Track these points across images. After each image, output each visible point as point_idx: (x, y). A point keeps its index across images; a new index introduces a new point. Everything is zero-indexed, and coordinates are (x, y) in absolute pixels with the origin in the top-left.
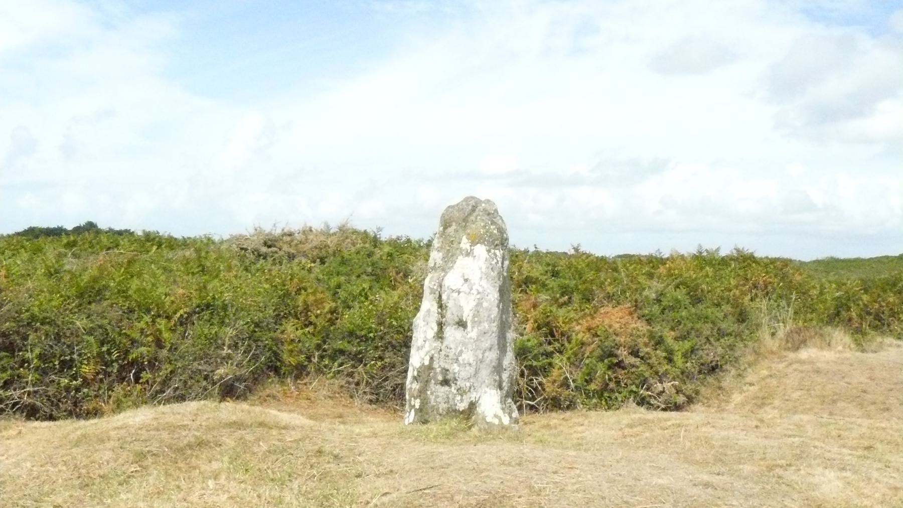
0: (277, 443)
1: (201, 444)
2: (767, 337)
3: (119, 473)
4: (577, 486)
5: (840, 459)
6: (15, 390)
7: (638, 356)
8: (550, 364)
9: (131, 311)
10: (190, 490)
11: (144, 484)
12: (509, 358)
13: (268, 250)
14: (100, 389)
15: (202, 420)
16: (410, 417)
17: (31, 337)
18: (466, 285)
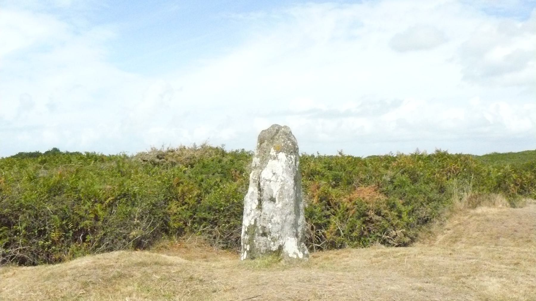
0: (166, 274)
1: (121, 276)
3: (73, 295)
4: (343, 293)
5: (499, 271)
6: (12, 249)
7: (380, 215)
8: (329, 222)
9: (80, 199)
12: (302, 219)
13: (159, 160)
14: (62, 246)
15: (122, 261)
16: (244, 256)
17: (20, 217)
18: (274, 177)
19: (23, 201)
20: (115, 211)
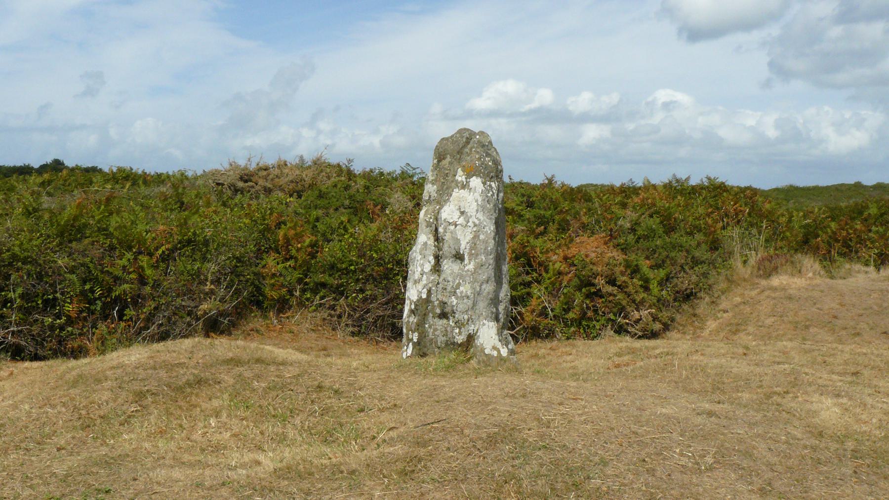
0: (276, 379)
2: (739, 264)
3: (120, 413)
8: (529, 294)
9: (112, 248)
14: (84, 326)
17: (13, 277)
19: (17, 249)
20: (173, 269)
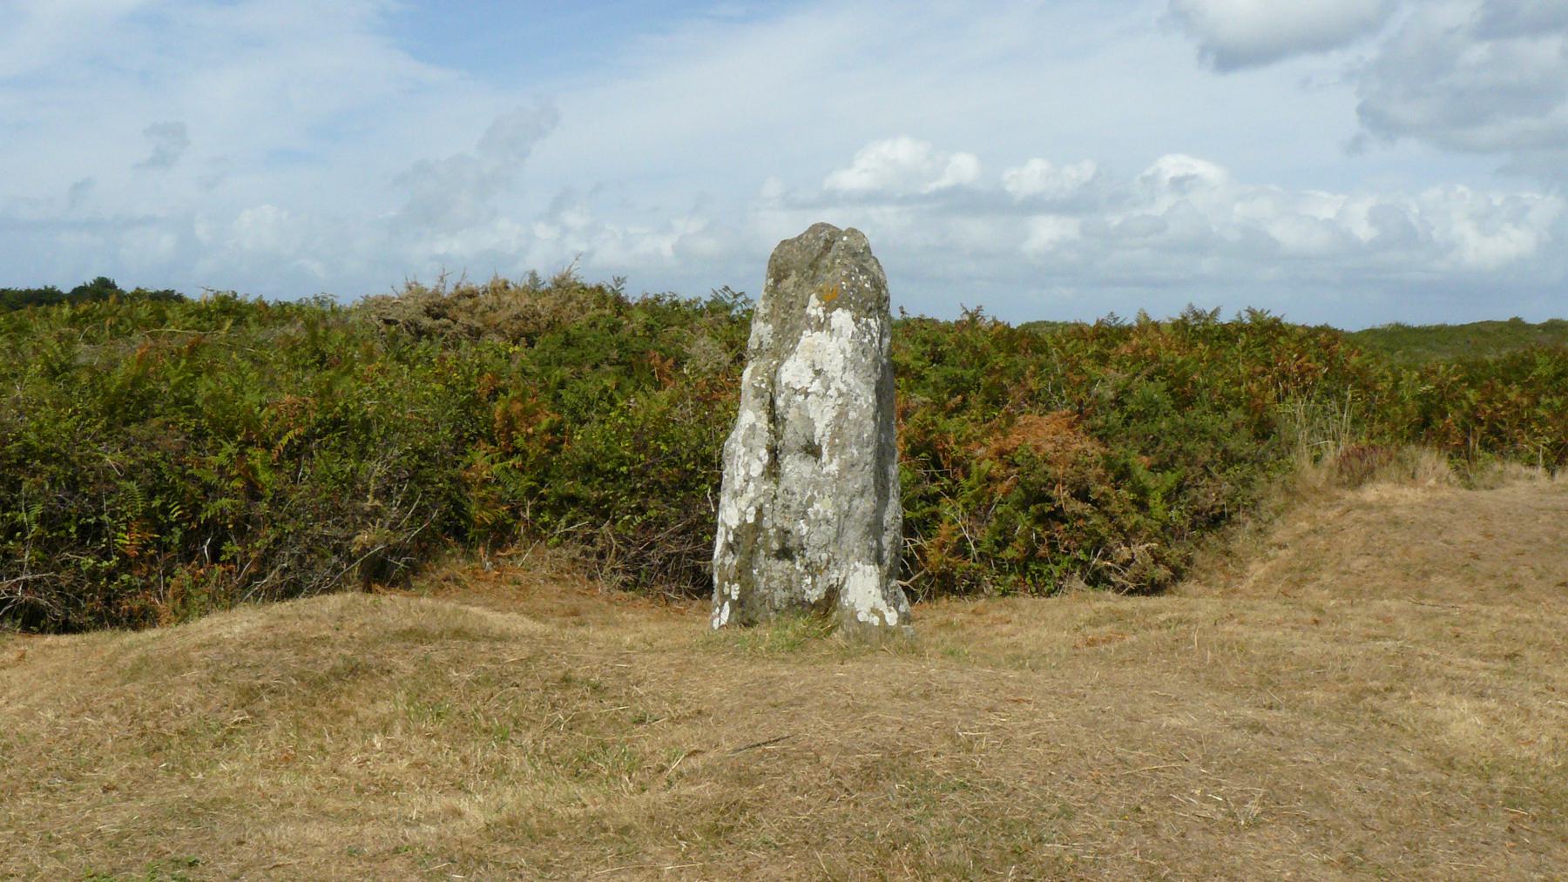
0: (490, 666)
1: (354, 671)
2: (1306, 463)
3: (213, 725)
7: (1085, 499)
8: (935, 515)
10: (342, 753)
11: (260, 746)
13: (432, 324)
14: (150, 573)
17: (25, 486)
19: (32, 436)
20: (308, 471)
